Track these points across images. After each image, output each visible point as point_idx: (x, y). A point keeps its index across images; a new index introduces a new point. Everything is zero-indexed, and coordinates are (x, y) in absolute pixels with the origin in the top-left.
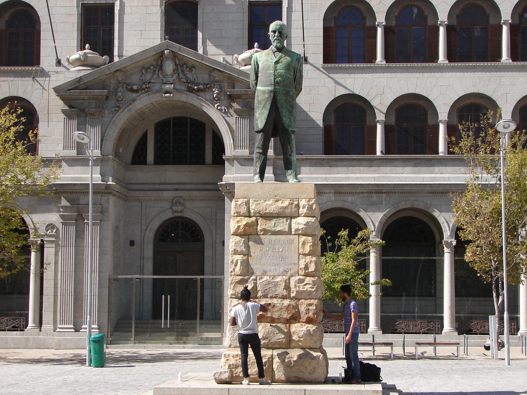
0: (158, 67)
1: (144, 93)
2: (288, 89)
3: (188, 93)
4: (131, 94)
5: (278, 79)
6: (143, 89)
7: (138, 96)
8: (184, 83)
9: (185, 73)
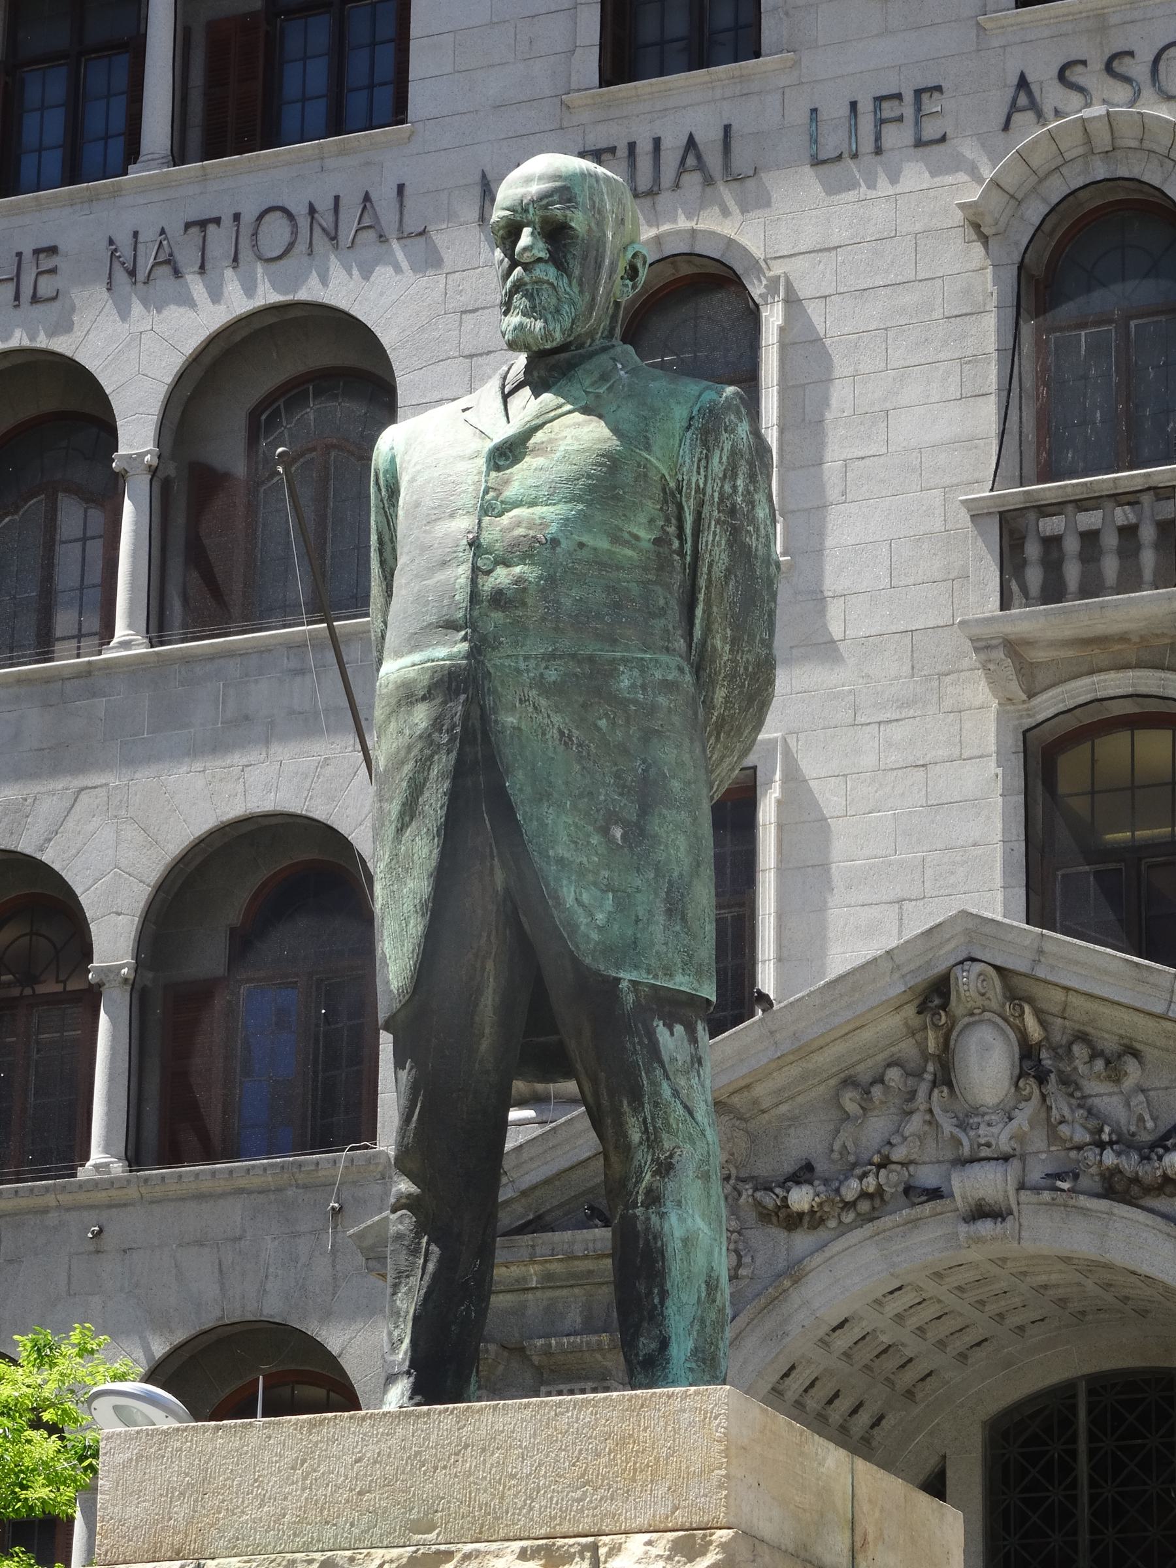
0: (930, 1068)
1: (851, 1227)
2: (591, 648)
3: (1103, 1204)
4: (781, 1235)
5: (502, 577)
6: (849, 1205)
7: (822, 1247)
8: (1079, 1148)
9: (1087, 1092)
